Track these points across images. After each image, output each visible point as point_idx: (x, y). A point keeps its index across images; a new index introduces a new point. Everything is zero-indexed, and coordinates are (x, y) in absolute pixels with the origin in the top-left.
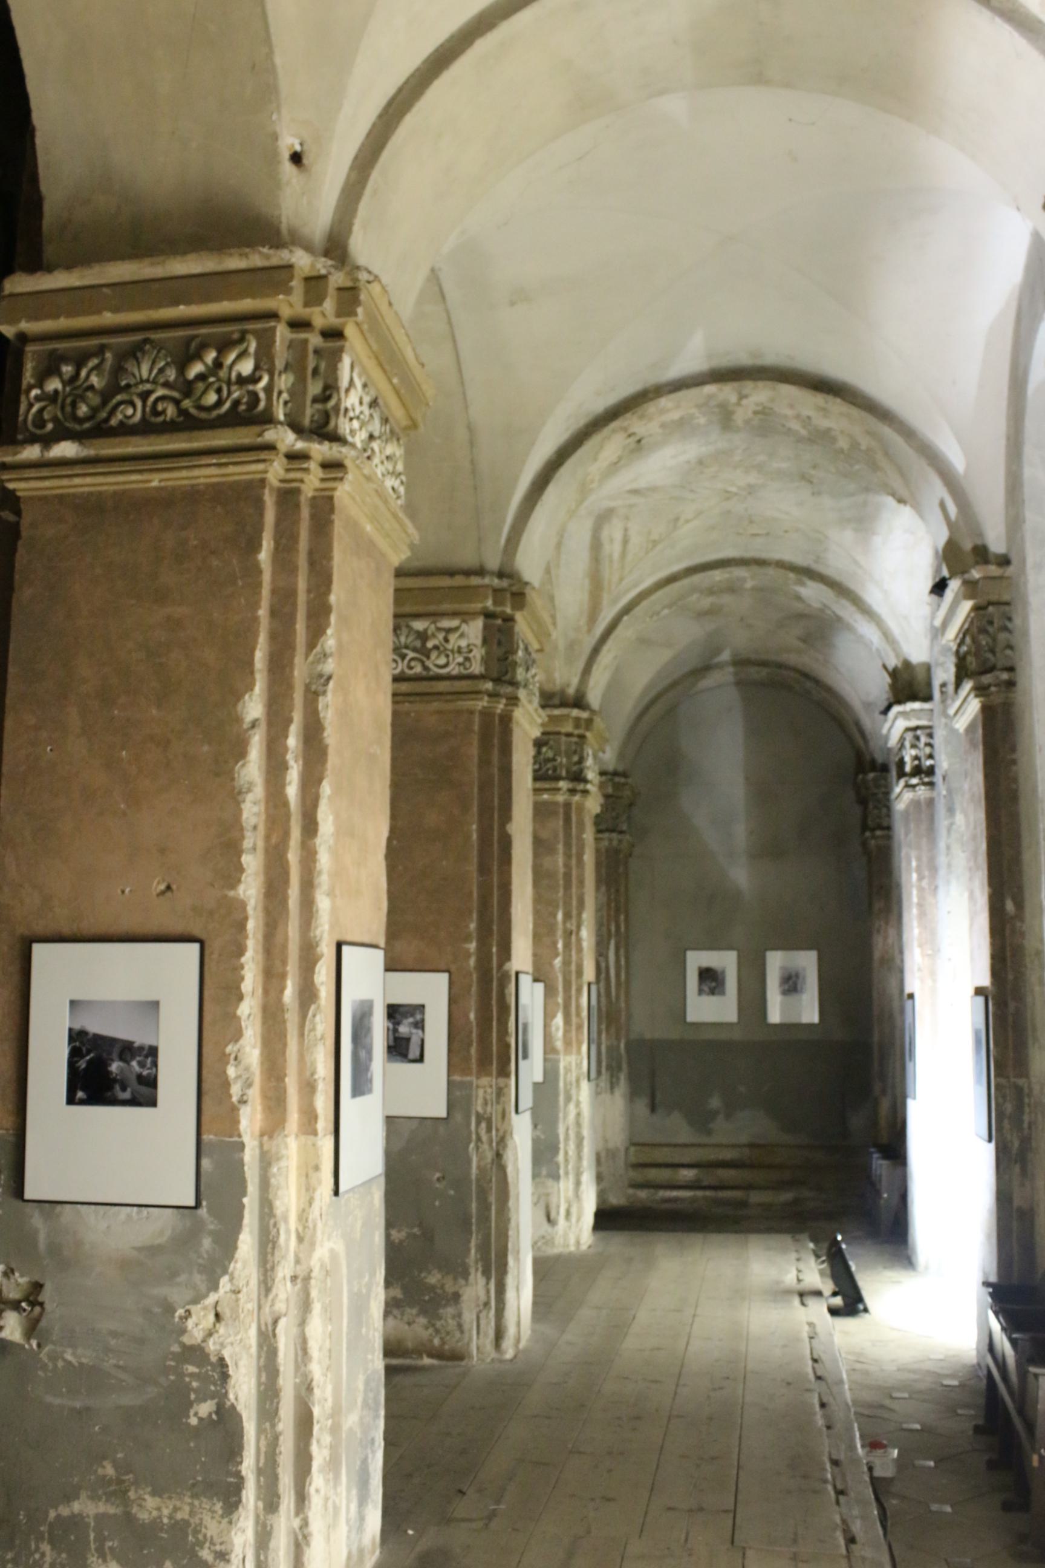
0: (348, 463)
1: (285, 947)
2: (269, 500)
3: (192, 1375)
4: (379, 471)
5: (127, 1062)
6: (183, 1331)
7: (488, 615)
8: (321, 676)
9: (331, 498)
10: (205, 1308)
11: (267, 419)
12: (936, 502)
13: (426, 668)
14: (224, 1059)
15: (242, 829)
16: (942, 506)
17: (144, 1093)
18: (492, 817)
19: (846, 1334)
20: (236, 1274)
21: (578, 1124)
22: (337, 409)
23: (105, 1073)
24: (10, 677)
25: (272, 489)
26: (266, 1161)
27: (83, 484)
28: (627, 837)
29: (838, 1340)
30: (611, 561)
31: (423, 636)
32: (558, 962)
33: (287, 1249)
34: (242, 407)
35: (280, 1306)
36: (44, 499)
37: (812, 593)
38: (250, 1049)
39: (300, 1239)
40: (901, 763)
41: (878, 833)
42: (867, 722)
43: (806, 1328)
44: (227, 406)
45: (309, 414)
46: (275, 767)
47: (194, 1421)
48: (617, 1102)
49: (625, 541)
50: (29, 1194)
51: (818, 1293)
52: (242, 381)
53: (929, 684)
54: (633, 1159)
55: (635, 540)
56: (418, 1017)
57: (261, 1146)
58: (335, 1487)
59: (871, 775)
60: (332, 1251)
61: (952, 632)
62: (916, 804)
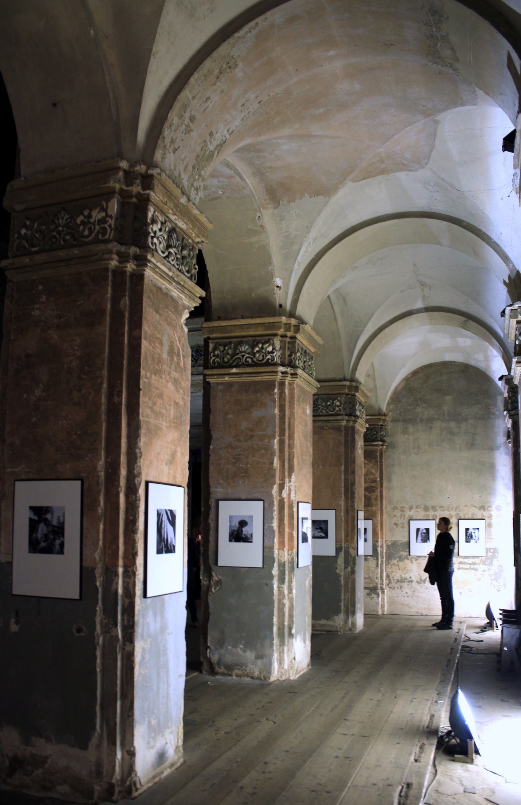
23: (239, 535)
50: (220, 564)
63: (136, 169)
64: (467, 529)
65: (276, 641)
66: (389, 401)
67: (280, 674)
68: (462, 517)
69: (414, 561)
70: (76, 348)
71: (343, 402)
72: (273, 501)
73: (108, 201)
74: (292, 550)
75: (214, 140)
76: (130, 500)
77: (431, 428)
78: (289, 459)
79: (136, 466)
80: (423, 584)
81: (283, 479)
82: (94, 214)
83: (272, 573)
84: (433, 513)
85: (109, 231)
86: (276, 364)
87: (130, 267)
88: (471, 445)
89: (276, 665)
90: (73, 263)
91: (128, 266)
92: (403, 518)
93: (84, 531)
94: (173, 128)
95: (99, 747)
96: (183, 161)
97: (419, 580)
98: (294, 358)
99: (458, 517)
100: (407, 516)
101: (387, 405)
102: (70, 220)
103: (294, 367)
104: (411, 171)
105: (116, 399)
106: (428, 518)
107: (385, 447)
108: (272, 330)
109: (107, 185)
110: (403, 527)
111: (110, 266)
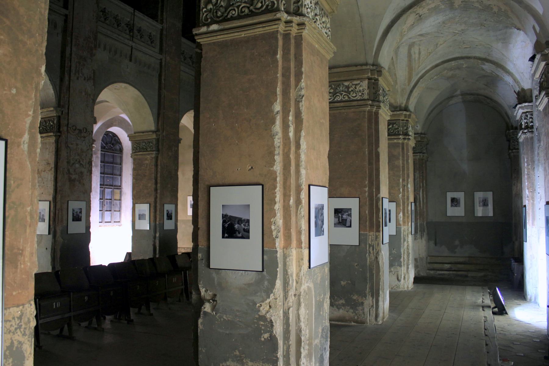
0: (306, 23)
1: (290, 186)
2: (280, 38)
3: (262, 325)
4: (320, 26)
5: (240, 225)
6: (259, 311)
7: (369, 79)
8: (300, 96)
9: (301, 35)
10: (266, 304)
11: (278, 10)
12: (532, 27)
13: (349, 98)
14: (270, 223)
15: (275, 147)
16: (534, 28)
17: (246, 235)
18: (373, 146)
19: (499, 321)
20: (275, 293)
21: (408, 249)
22: (302, 5)
23: (234, 228)
24: (201, 102)
25: (281, 34)
26: (285, 257)
27: (221, 38)
28: (426, 155)
29: (496, 323)
30: (415, 61)
31: (348, 87)
32: (400, 195)
33: (293, 286)
34: (270, 7)
35: (291, 304)
36: (209, 44)
37: (487, 67)
38: (279, 220)
39: (297, 282)
40: (521, 124)
41: (514, 151)
42: (509, 113)
43: (484, 318)
44: (265, 7)
45: (292, 8)
46: (285, 127)
47: (263, 339)
48: (423, 243)
49: (420, 53)
51: (489, 307)
53: (531, 96)
54: (429, 261)
55: (423, 53)
56: (349, 212)
57: (284, 252)
58: (310, 363)
59: (511, 131)
60: (308, 287)
61: (538, 75)
62: (526, 139)
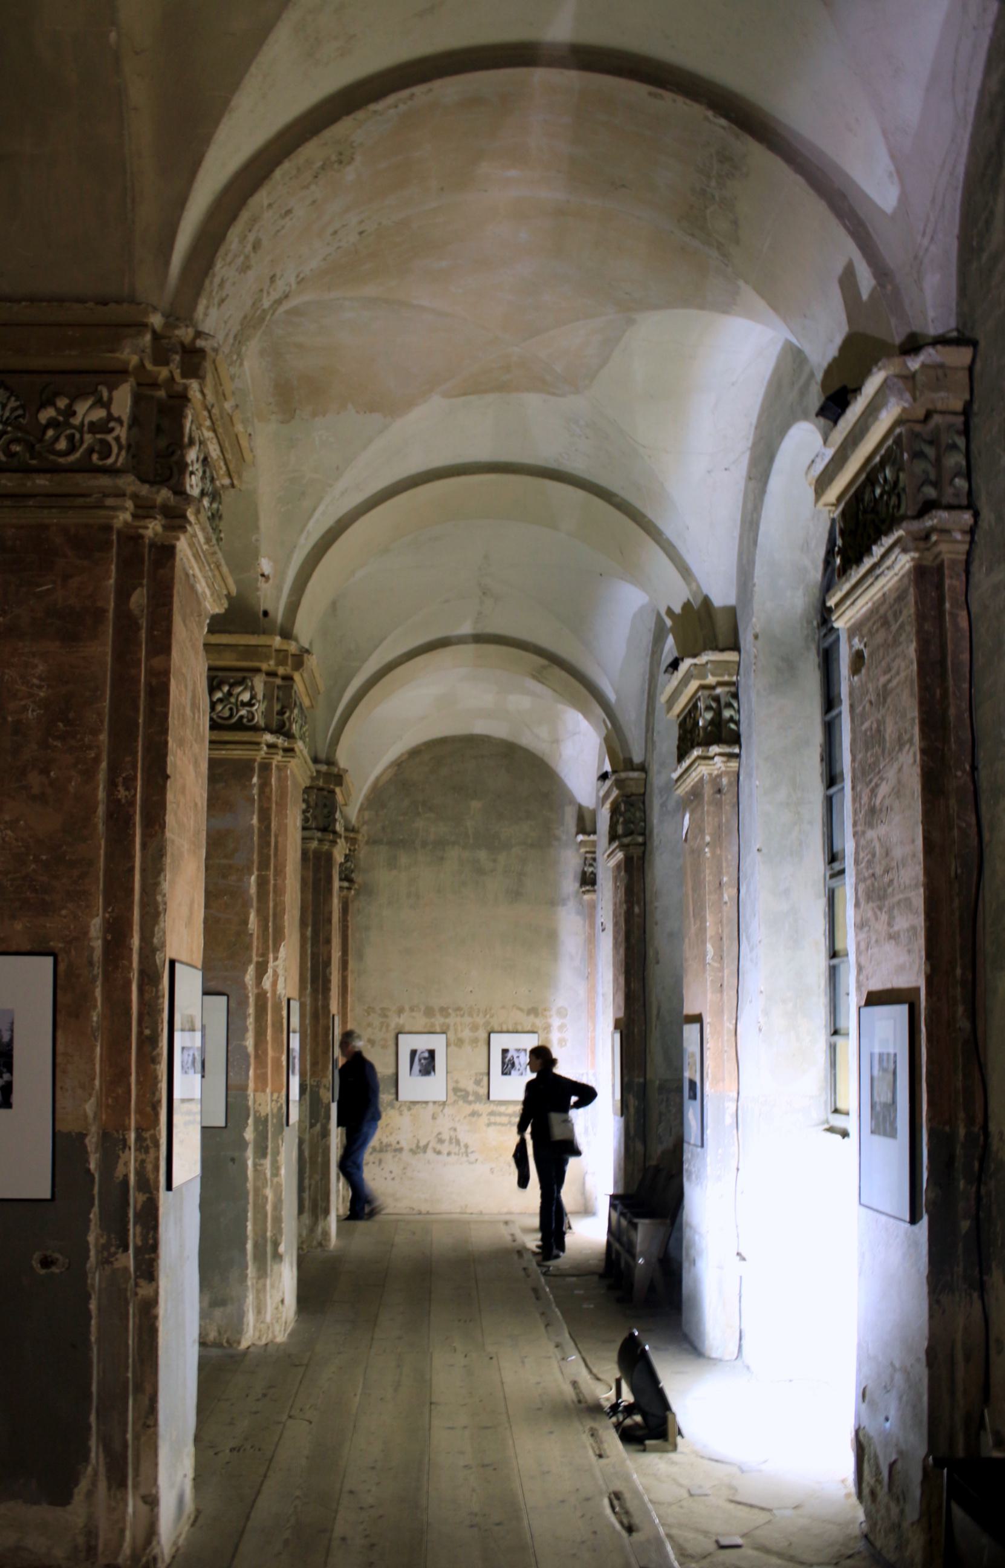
52: (244, 704)
63: (177, 332)
64: (505, 1052)
65: (251, 1271)
66: (362, 805)
67: (257, 1334)
68: (496, 1028)
69: (405, 1112)
70: (35, 681)
71: (312, 803)
72: (247, 997)
73: (112, 388)
74: (280, 1092)
75: (275, 290)
76: (147, 996)
77: (442, 859)
78: (275, 915)
79: (156, 929)
80: (422, 1154)
81: (264, 954)
82: (81, 408)
83: (243, 1138)
84: (442, 1020)
85: (115, 450)
86: (255, 729)
87: (153, 528)
88: (516, 895)
89: (250, 1317)
90: (31, 503)
91: (151, 526)
92: (384, 1029)
93: (59, 1059)
94: (228, 259)
95: (90, 1494)
96: (226, 322)
97: (414, 1146)
98: (289, 718)
99: (489, 1029)
100: (393, 1025)
101: (360, 811)
102: (20, 412)
103: (289, 736)
104: (554, 394)
105: (122, 793)
106: (432, 1030)
107: (353, 892)
108: (251, 661)
109: (117, 355)
110: (384, 1047)
111: (115, 521)
